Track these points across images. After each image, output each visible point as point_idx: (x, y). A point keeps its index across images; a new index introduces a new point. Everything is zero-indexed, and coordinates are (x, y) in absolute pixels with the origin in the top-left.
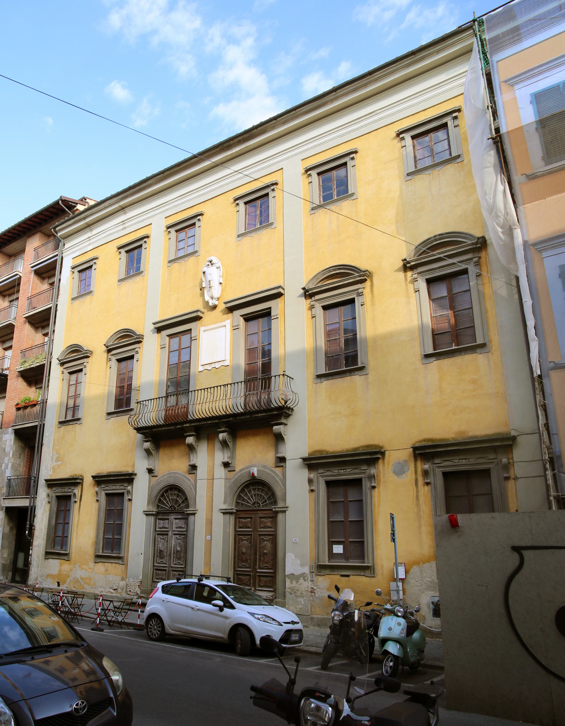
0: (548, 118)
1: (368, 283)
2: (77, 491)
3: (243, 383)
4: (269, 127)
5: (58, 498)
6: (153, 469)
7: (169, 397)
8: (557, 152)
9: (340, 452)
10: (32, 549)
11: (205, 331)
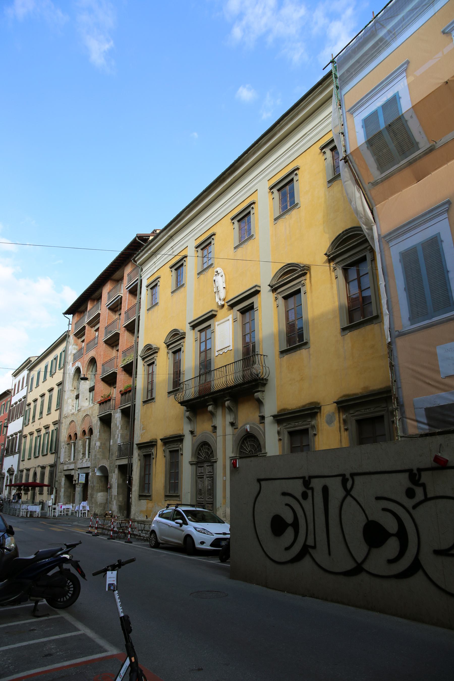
0: (380, 133)
1: (308, 275)
2: (154, 451)
3: (241, 361)
4: (245, 159)
5: (291, 434)
6: (193, 431)
7: (201, 376)
8: (385, 163)
9: (295, 409)
10: (131, 494)
11: (218, 325)
